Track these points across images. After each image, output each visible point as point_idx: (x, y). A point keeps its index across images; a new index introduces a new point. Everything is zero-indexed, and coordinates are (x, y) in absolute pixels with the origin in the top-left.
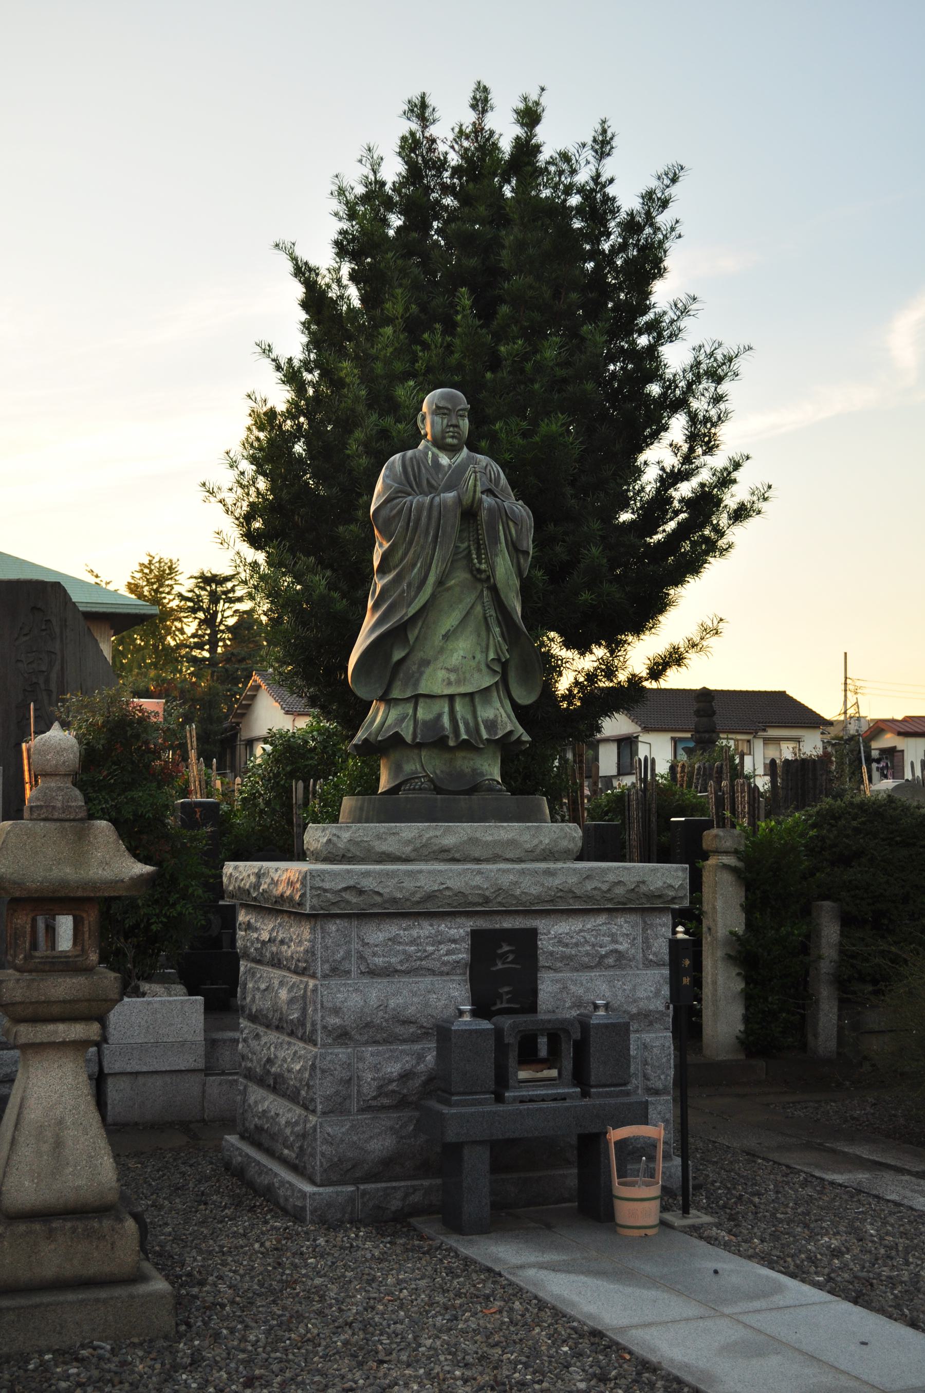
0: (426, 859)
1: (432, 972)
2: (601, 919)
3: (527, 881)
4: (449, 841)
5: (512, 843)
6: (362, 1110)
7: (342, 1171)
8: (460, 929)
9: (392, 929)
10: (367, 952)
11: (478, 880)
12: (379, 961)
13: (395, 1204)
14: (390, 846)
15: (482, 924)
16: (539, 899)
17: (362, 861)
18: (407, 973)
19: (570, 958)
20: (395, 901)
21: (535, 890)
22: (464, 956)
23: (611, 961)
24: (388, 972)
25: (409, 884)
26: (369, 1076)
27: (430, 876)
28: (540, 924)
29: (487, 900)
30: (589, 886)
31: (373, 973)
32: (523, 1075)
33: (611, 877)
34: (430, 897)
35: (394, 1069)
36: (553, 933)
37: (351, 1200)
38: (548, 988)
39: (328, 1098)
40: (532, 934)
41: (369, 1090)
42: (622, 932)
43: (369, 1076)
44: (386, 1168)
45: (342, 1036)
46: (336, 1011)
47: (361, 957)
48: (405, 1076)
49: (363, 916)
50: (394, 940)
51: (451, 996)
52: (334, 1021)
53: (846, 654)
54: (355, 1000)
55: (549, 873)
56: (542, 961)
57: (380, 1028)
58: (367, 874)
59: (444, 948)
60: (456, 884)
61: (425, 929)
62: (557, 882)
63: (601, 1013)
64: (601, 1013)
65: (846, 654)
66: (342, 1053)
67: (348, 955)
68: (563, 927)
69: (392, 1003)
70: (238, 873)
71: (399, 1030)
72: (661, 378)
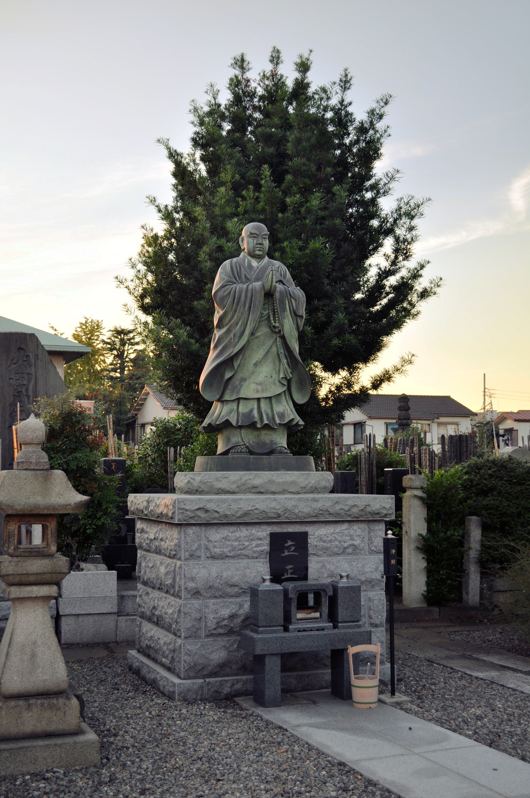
0: (244, 492)
1: (247, 557)
2: (345, 526)
3: (302, 505)
5: (293, 483)
6: (208, 636)
7: (197, 671)
9: (225, 532)
10: (210, 545)
11: (274, 504)
12: (217, 551)
13: (226, 690)
14: (223, 485)
17: (208, 493)
18: (233, 557)
19: (327, 549)
20: (226, 516)
21: (306, 510)
23: (350, 550)
24: (223, 557)
25: (235, 507)
26: (211, 616)
27: (246, 503)
29: (279, 516)
30: (338, 507)
32: (300, 615)
33: (350, 503)
34: (246, 514)
35: (226, 612)
36: (317, 535)
37: (201, 687)
38: (314, 566)
39: (188, 629)
40: (305, 535)
41: (211, 624)
43: (211, 616)
44: (221, 669)
45: (196, 593)
47: (207, 548)
49: (207, 525)
51: (259, 571)
57: (218, 589)
59: (254, 543)
62: (319, 505)
63: (345, 580)
66: (196, 603)
69: (225, 575)
70: (136, 501)
71: (229, 590)
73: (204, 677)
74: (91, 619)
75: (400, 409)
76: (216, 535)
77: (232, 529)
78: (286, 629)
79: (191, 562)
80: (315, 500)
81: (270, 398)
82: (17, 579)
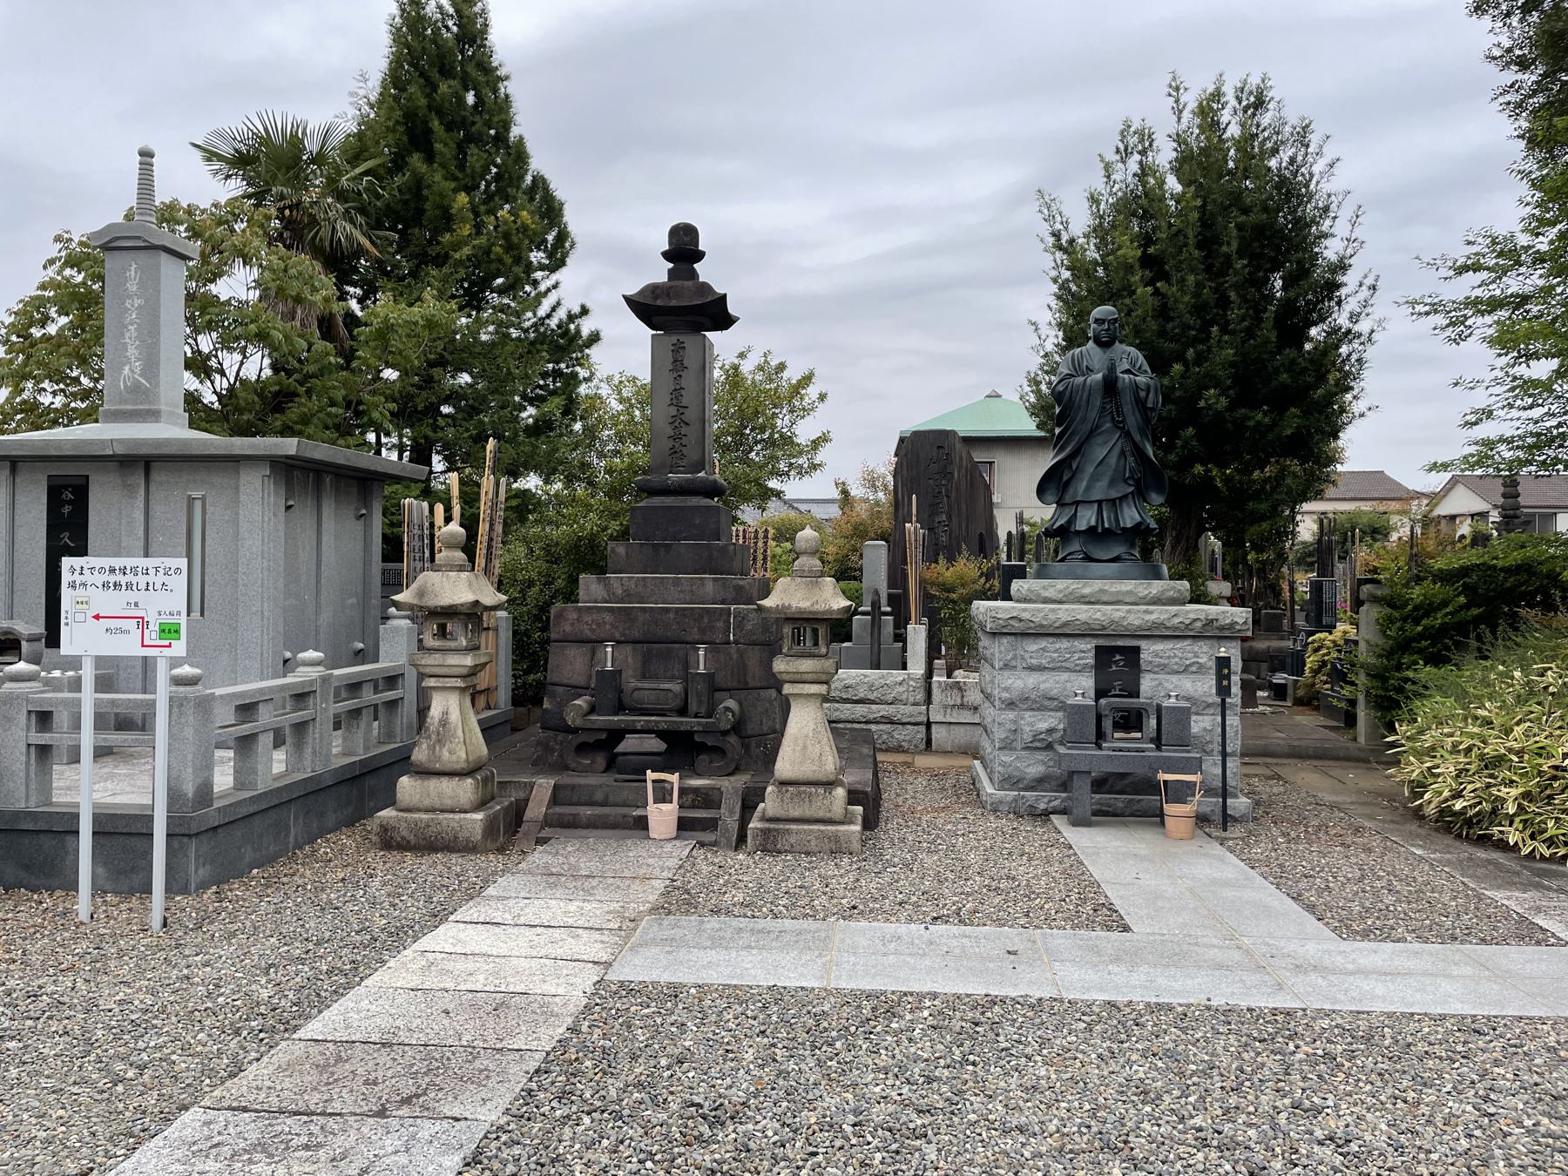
0: (1072, 602)
1: (1068, 670)
2: (1188, 642)
3: (1136, 617)
4: (1087, 591)
5: (1129, 593)
6: (1024, 749)
7: (1010, 781)
8: (1088, 645)
9: (1043, 643)
10: (1027, 656)
11: (1098, 615)
12: (1034, 662)
13: (1042, 806)
14: (1050, 594)
15: (1102, 642)
16: (1140, 628)
17: (1035, 602)
18: (1054, 669)
19: (1165, 666)
20: (1042, 626)
21: (1137, 623)
22: (1092, 661)
23: (1194, 669)
24: (1040, 669)
25: (1052, 617)
26: (1027, 729)
27: (1083, 613)
28: (1143, 644)
29: (1104, 628)
30: (1176, 620)
31: (1031, 668)
32: (1117, 735)
33: (1193, 616)
34: (1066, 624)
35: (1044, 726)
36: (1150, 651)
37: (1015, 800)
38: (1147, 684)
39: (1002, 740)
40: (1137, 650)
41: (1028, 737)
42: (1205, 654)
43: (1027, 729)
44: (1039, 783)
45: (1011, 705)
46: (1006, 689)
47: (1023, 658)
48: (1050, 731)
49: (1024, 635)
50: (1043, 649)
51: (1081, 687)
52: (1005, 695)
53: (146, 154)
54: (1019, 684)
55: (1147, 612)
56: (1143, 666)
57: (1035, 701)
58: (1025, 610)
59: (1077, 656)
60: (1082, 617)
61: (1064, 644)
62: (1153, 617)
63: (1173, 700)
64: (1173, 700)
65: (146, 154)
66: (1011, 715)
67: (1015, 658)
68: (1159, 646)
69: (1042, 687)
70: (980, 607)
71: (1047, 703)
72: (1144, 253)
73: (1020, 790)
74: (962, 729)
75: (1504, 496)
76: (1033, 646)
77: (1051, 640)
78: (1100, 748)
79: (1006, 673)
80: (1147, 612)
81: (1113, 501)
82: (815, 677)
